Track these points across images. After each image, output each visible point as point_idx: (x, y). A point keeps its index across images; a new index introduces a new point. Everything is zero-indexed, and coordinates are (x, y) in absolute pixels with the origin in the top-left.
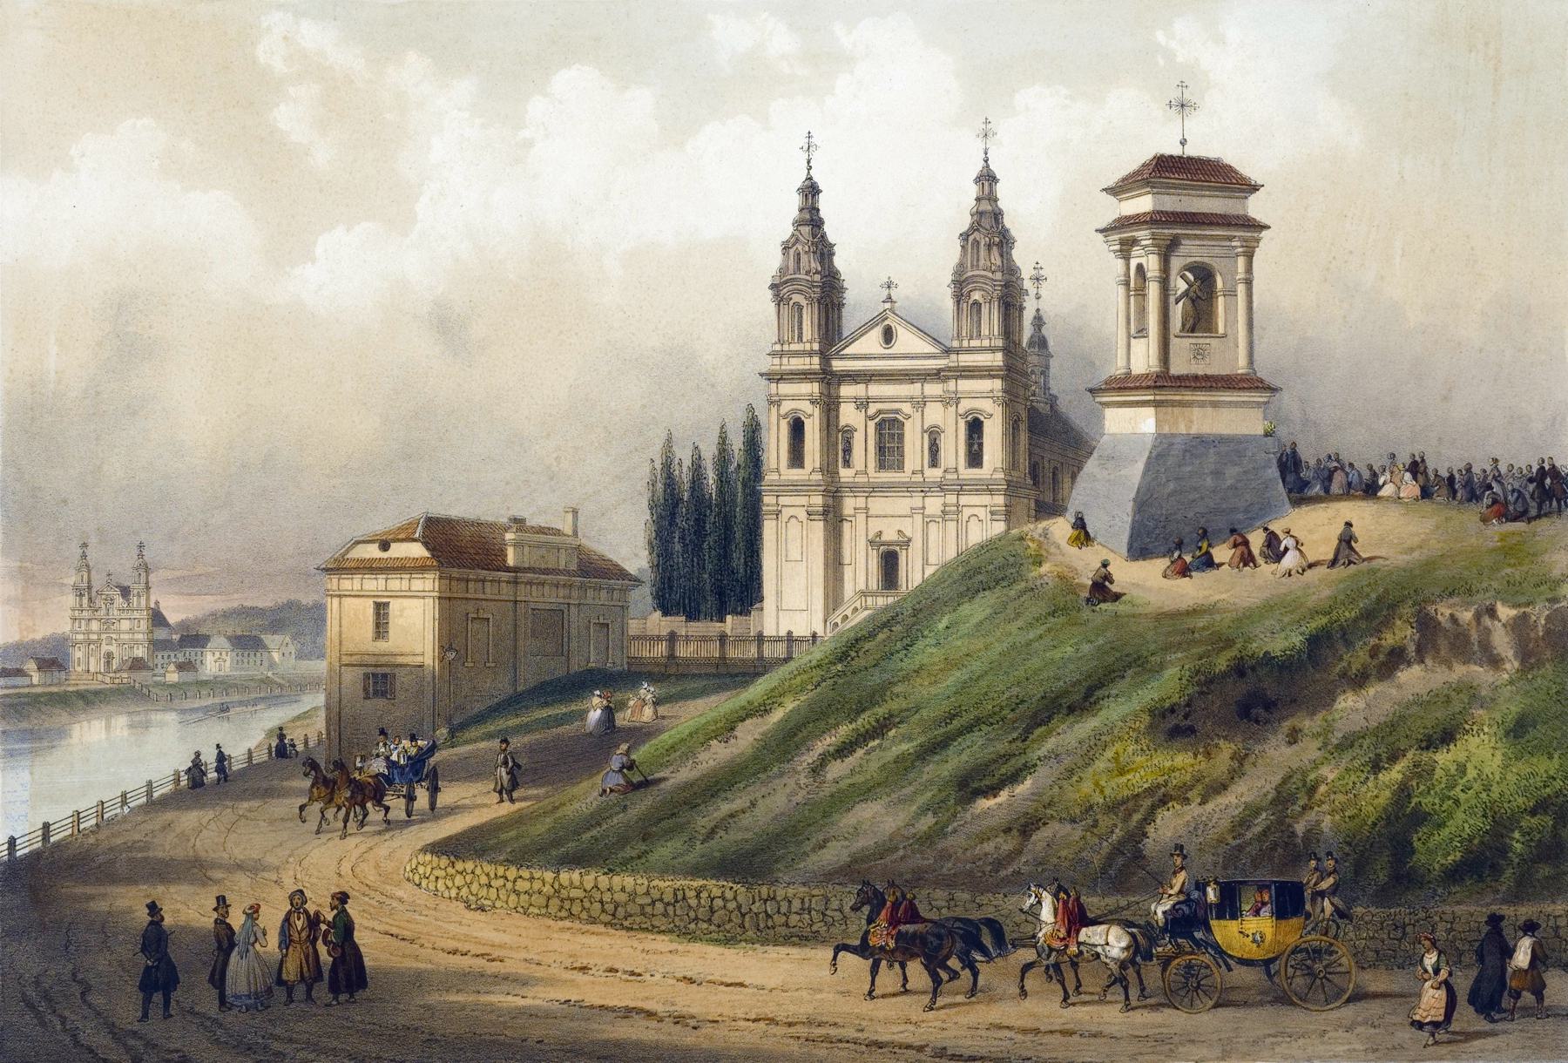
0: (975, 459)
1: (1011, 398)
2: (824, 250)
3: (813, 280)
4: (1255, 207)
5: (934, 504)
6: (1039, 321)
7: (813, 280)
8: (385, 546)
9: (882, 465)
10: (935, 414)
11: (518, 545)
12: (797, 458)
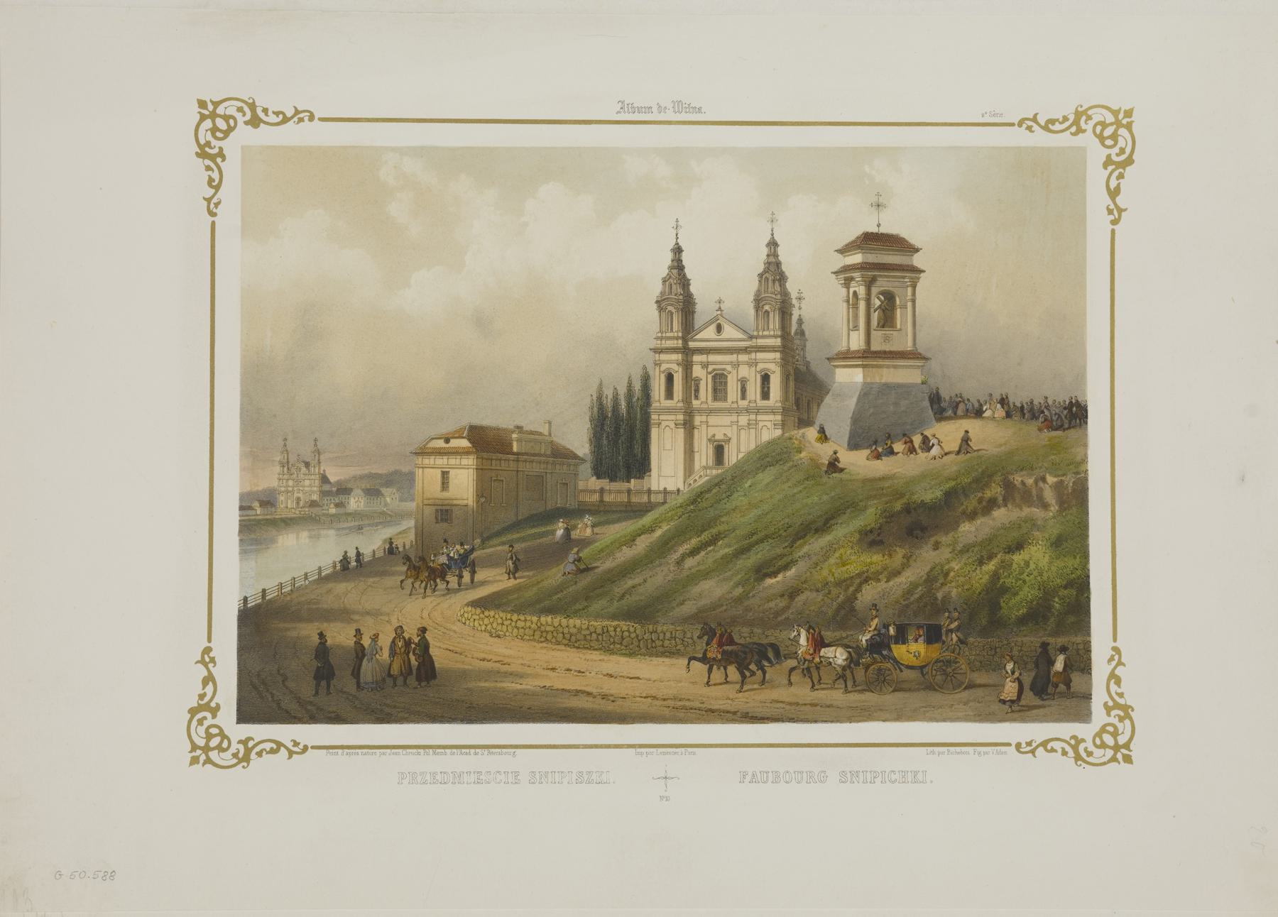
0: (765, 395)
1: (785, 363)
2: (685, 283)
3: (679, 299)
4: (917, 260)
5: (743, 420)
6: (800, 321)
7: (679, 299)
8: (447, 441)
9: (715, 399)
10: (744, 371)
11: (519, 440)
12: (669, 394)
